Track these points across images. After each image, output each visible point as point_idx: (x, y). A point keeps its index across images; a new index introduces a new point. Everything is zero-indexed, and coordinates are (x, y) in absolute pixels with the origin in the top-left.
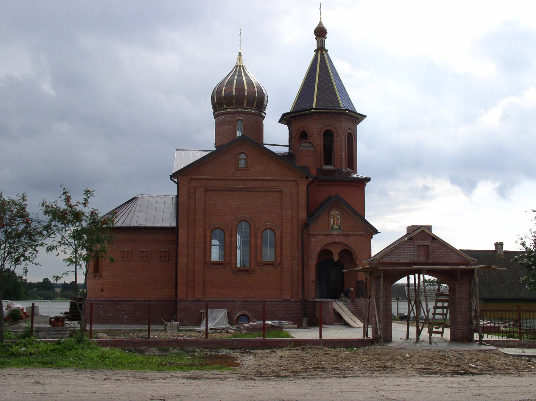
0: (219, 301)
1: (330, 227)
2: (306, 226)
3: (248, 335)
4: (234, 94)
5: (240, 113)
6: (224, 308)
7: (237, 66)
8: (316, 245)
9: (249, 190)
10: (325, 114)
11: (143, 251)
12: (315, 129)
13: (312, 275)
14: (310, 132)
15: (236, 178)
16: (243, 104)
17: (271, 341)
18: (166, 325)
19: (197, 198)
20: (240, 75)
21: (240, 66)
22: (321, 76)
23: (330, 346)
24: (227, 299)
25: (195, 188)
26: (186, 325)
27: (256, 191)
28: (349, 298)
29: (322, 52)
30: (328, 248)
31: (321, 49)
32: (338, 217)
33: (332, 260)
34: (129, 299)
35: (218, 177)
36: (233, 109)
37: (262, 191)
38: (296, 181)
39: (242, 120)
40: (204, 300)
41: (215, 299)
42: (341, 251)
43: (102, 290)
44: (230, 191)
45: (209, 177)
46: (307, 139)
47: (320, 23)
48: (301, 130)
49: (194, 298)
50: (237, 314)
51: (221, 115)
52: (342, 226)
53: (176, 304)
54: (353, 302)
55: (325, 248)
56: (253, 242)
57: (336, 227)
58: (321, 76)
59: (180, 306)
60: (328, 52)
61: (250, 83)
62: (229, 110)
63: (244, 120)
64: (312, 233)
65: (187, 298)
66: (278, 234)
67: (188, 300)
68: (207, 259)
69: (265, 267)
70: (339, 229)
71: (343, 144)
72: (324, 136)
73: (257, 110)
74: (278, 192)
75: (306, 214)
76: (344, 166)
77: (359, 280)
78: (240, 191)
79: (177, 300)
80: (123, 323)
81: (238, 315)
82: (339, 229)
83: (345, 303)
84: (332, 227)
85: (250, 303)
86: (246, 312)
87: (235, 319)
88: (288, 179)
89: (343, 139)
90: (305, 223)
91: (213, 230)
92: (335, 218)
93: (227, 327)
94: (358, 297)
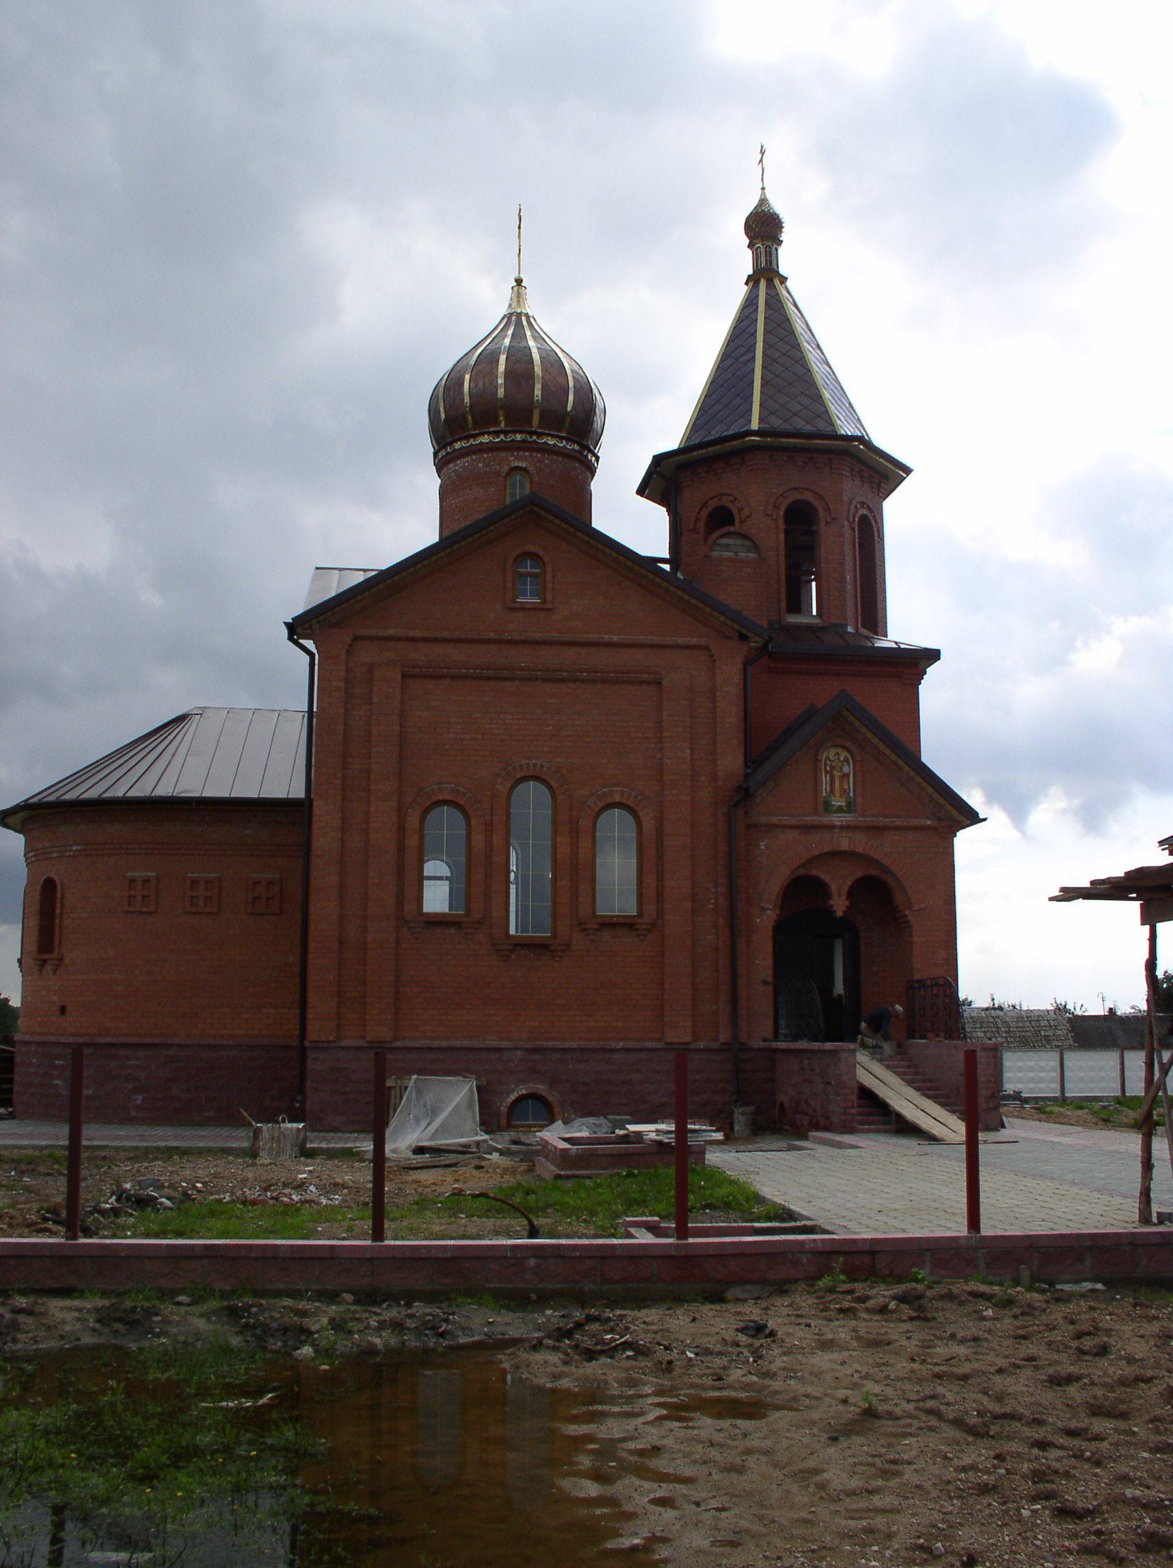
0: (449, 1048)
1: (820, 800)
2: (743, 795)
3: (569, 1184)
4: (501, 392)
5: (518, 449)
6: (463, 1072)
7: (511, 314)
8: (777, 860)
9: (552, 677)
10: (786, 469)
11: (194, 882)
12: (758, 498)
13: (761, 962)
14: (741, 510)
15: (506, 636)
16: (529, 420)
17: (722, 1255)
18: (257, 1132)
19: (375, 700)
20: (519, 335)
21: (519, 315)
22: (767, 345)
23: (1025, 1274)
24: (476, 1043)
25: (371, 668)
26: (336, 1130)
27: (576, 680)
28: (886, 1038)
29: (770, 282)
30: (814, 872)
31: (766, 274)
32: (846, 769)
33: (829, 912)
34: (148, 1040)
35: (446, 634)
36: (497, 433)
37: (594, 681)
38: (707, 648)
39: (525, 470)
40: (399, 1044)
41: (436, 1044)
42: (851, 887)
43: (63, 1010)
44: (489, 678)
45: (418, 633)
46: (733, 524)
47: (763, 201)
48: (712, 504)
49: (363, 1037)
50: (508, 1093)
51: (460, 457)
52: (859, 800)
53: (303, 1059)
54: (901, 1050)
55: (803, 872)
56: (564, 850)
57: (838, 802)
58: (767, 345)
59: (317, 1064)
60: (788, 283)
61: (553, 363)
62: (485, 439)
63: (532, 469)
64: (762, 820)
65: (338, 1038)
66: (649, 824)
67: (344, 1043)
68: (409, 907)
69: (606, 935)
70: (850, 807)
71: (848, 548)
72: (786, 523)
73: (574, 442)
74: (648, 683)
75: (741, 758)
76: (851, 620)
77: (917, 976)
78: (522, 679)
79: (307, 1044)
80: (127, 1120)
81: (513, 1097)
82: (850, 807)
83: (875, 1051)
84: (827, 804)
85: (556, 1056)
86: (541, 1088)
87: (504, 1109)
88: (681, 640)
89: (847, 532)
90: (739, 788)
91: (427, 811)
92: (838, 775)
93: (478, 1143)
94: (911, 1035)
